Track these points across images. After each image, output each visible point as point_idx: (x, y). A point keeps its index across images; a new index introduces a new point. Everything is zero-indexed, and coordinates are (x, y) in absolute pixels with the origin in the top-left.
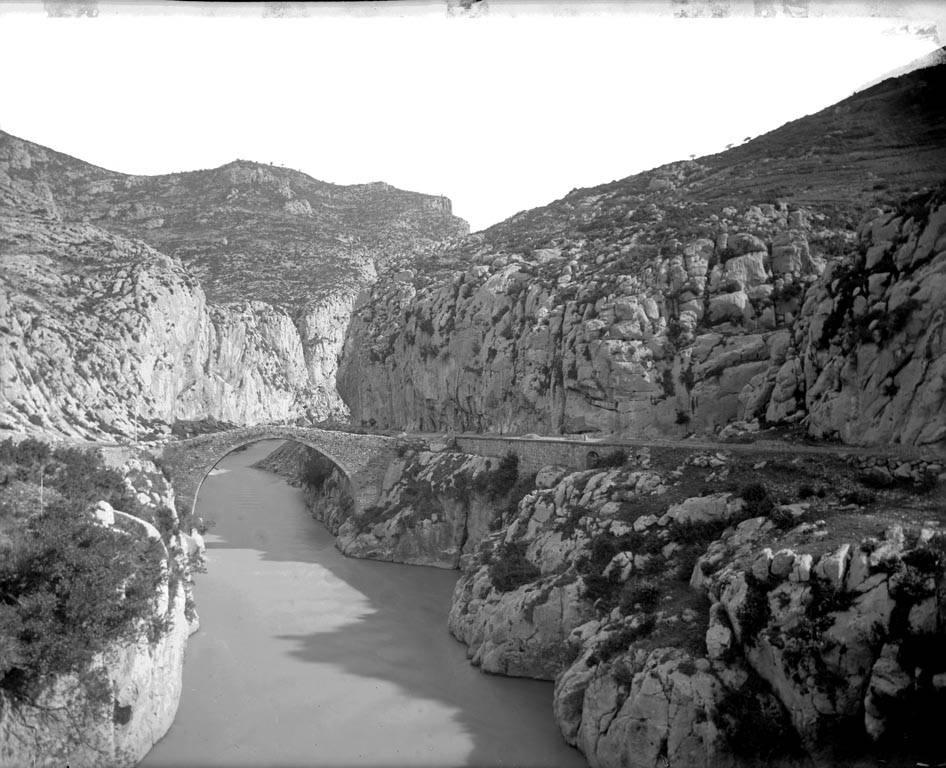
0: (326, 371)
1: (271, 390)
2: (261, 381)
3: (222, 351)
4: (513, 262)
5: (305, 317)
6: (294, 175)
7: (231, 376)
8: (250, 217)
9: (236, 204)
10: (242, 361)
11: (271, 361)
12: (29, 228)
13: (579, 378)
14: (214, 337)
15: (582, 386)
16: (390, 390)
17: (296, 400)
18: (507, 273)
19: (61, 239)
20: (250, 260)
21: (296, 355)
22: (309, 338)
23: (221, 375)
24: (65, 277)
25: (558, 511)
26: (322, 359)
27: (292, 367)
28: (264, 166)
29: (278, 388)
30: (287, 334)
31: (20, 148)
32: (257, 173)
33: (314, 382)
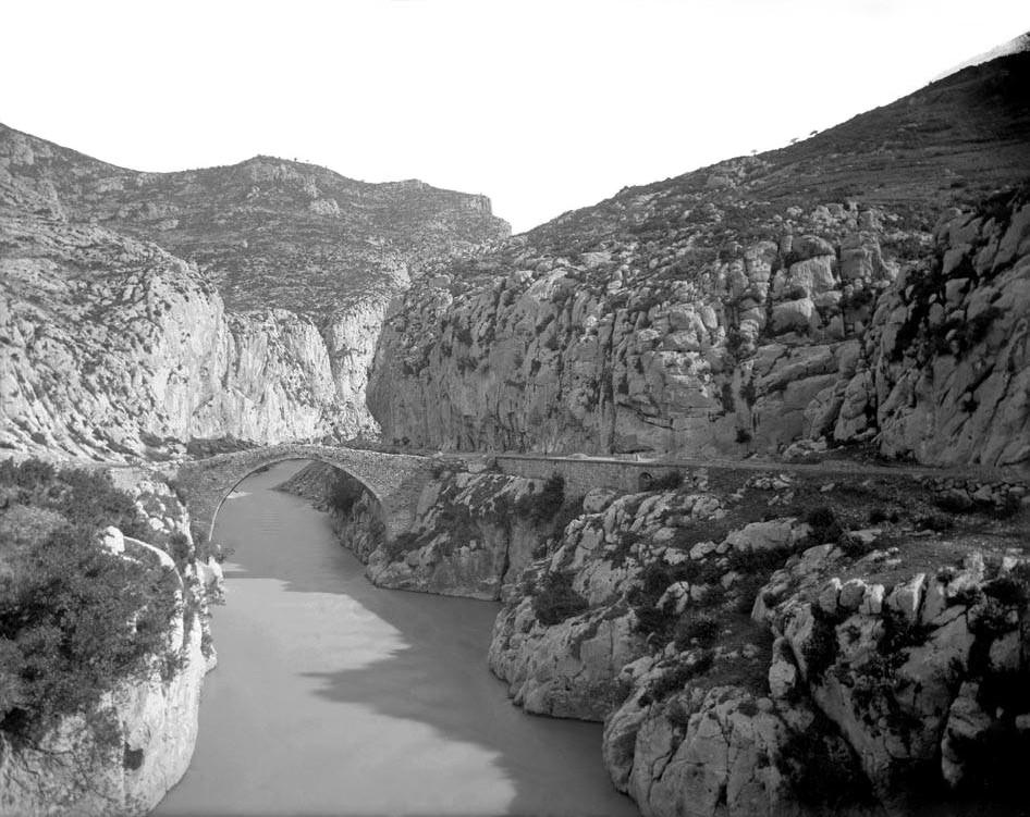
0: (355, 385)
1: (295, 406)
3: (241, 364)
4: (558, 267)
6: (319, 172)
7: (252, 391)
8: (272, 217)
9: (257, 203)
11: (296, 374)
12: (31, 230)
15: (634, 402)
16: (425, 406)
17: (323, 417)
18: (552, 279)
20: (272, 265)
21: (323, 368)
23: (240, 389)
24: (71, 282)
25: (608, 538)
26: (351, 372)
27: (318, 381)
28: (287, 162)
29: (303, 403)
30: (312, 346)
32: (280, 170)
33: (342, 397)
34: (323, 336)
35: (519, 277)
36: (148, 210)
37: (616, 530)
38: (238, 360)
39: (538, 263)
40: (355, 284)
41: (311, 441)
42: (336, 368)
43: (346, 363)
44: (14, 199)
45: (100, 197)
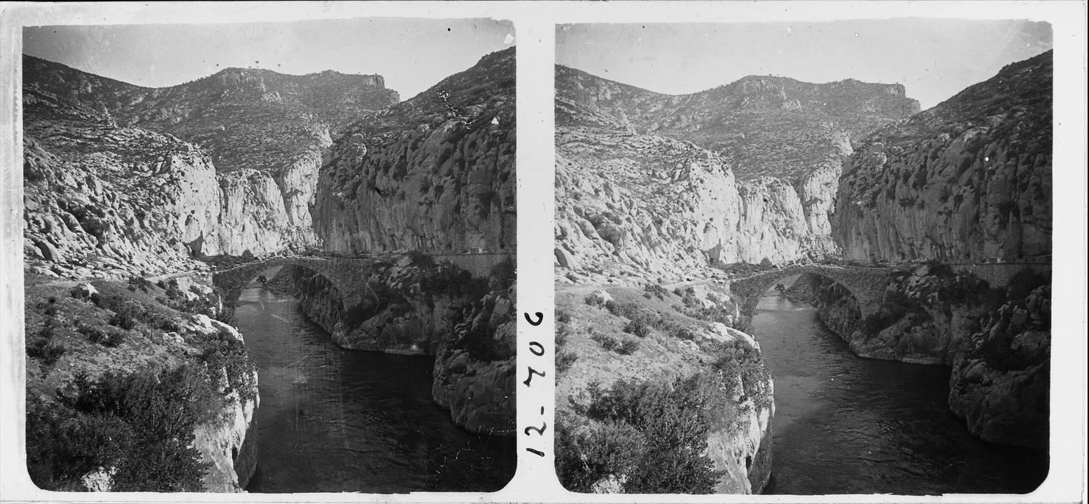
1: (782, 239)
2: (257, 226)
3: (748, 215)
4: (449, 118)
5: (283, 178)
6: (788, 81)
7: (237, 224)
10: (243, 213)
12: (98, 134)
13: (1034, 214)
14: (741, 205)
16: (876, 233)
18: (446, 128)
19: (637, 146)
22: (287, 192)
23: (230, 224)
24: (125, 164)
26: (817, 215)
28: (766, 78)
30: (792, 200)
31: (84, 79)
32: (761, 83)
34: (278, 184)
35: (421, 129)
36: (681, 120)
37: (1037, 310)
38: (746, 212)
39: (955, 127)
40: (821, 151)
41: (794, 262)
42: (807, 215)
43: (813, 208)
44: (85, 115)
45: (132, 108)
